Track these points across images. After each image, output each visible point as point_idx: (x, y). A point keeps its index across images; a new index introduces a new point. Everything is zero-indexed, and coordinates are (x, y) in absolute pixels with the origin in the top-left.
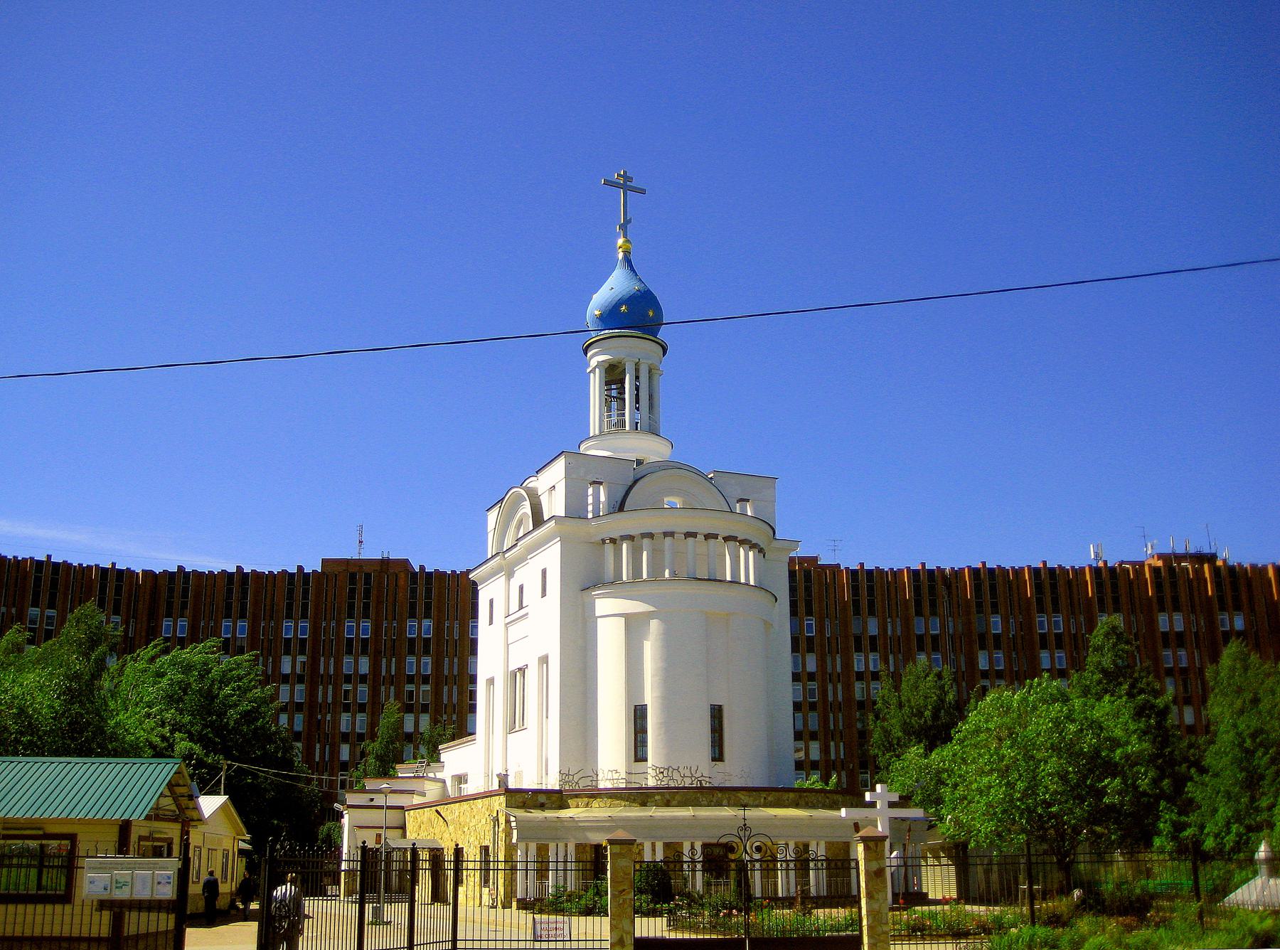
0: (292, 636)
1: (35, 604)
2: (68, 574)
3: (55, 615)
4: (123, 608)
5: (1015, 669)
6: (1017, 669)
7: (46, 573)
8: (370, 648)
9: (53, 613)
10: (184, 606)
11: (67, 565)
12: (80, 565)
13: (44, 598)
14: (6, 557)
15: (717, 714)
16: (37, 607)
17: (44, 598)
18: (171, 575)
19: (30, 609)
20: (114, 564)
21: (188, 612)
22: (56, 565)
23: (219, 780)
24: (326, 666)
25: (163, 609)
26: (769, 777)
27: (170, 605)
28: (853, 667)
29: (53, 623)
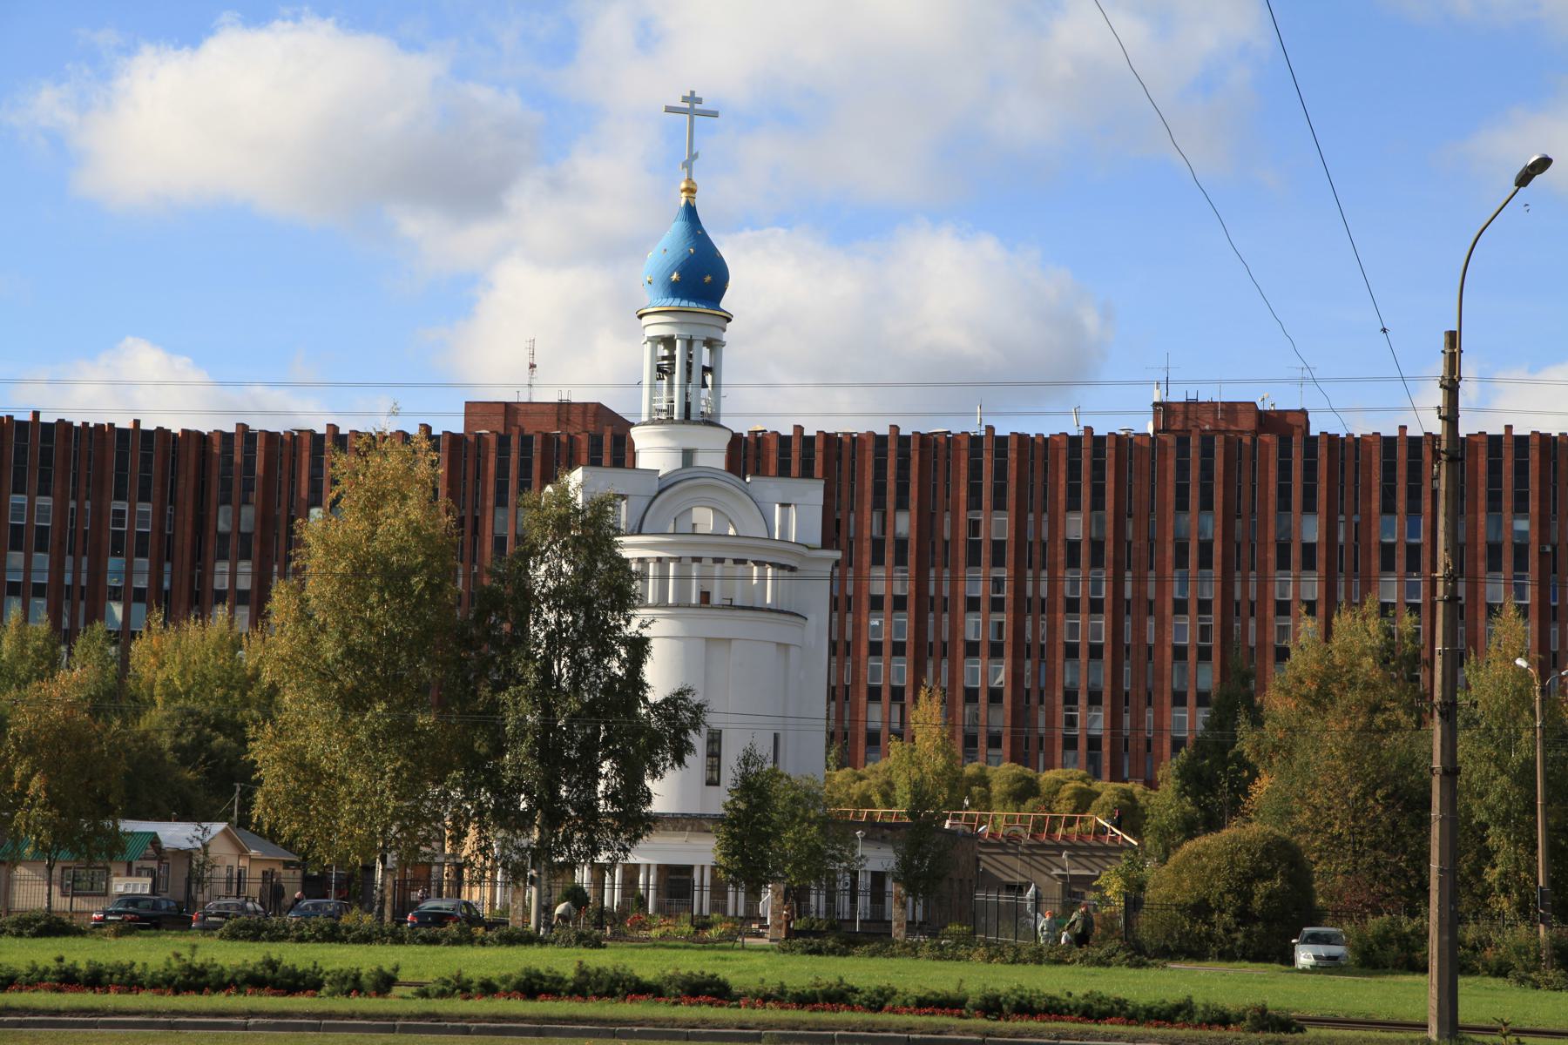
0: (126, 529)
1: (18, 489)
2: (67, 439)
3: (26, 502)
4: (155, 490)
5: (167, 532)
6: (171, 532)
7: (35, 443)
8: (255, 548)
9: (21, 499)
10: (248, 487)
11: (63, 425)
12: (1350, 435)
13: (33, 481)
14: (72, 423)
15: (776, 737)
16: (23, 492)
17: (33, 481)
18: (226, 438)
19: (12, 496)
20: (137, 422)
21: (255, 496)
22: (148, 434)
23: (234, 801)
24: (938, 627)
25: (215, 491)
26: (1057, 999)
27: (227, 486)
28: (1233, 593)
29: (124, 521)
